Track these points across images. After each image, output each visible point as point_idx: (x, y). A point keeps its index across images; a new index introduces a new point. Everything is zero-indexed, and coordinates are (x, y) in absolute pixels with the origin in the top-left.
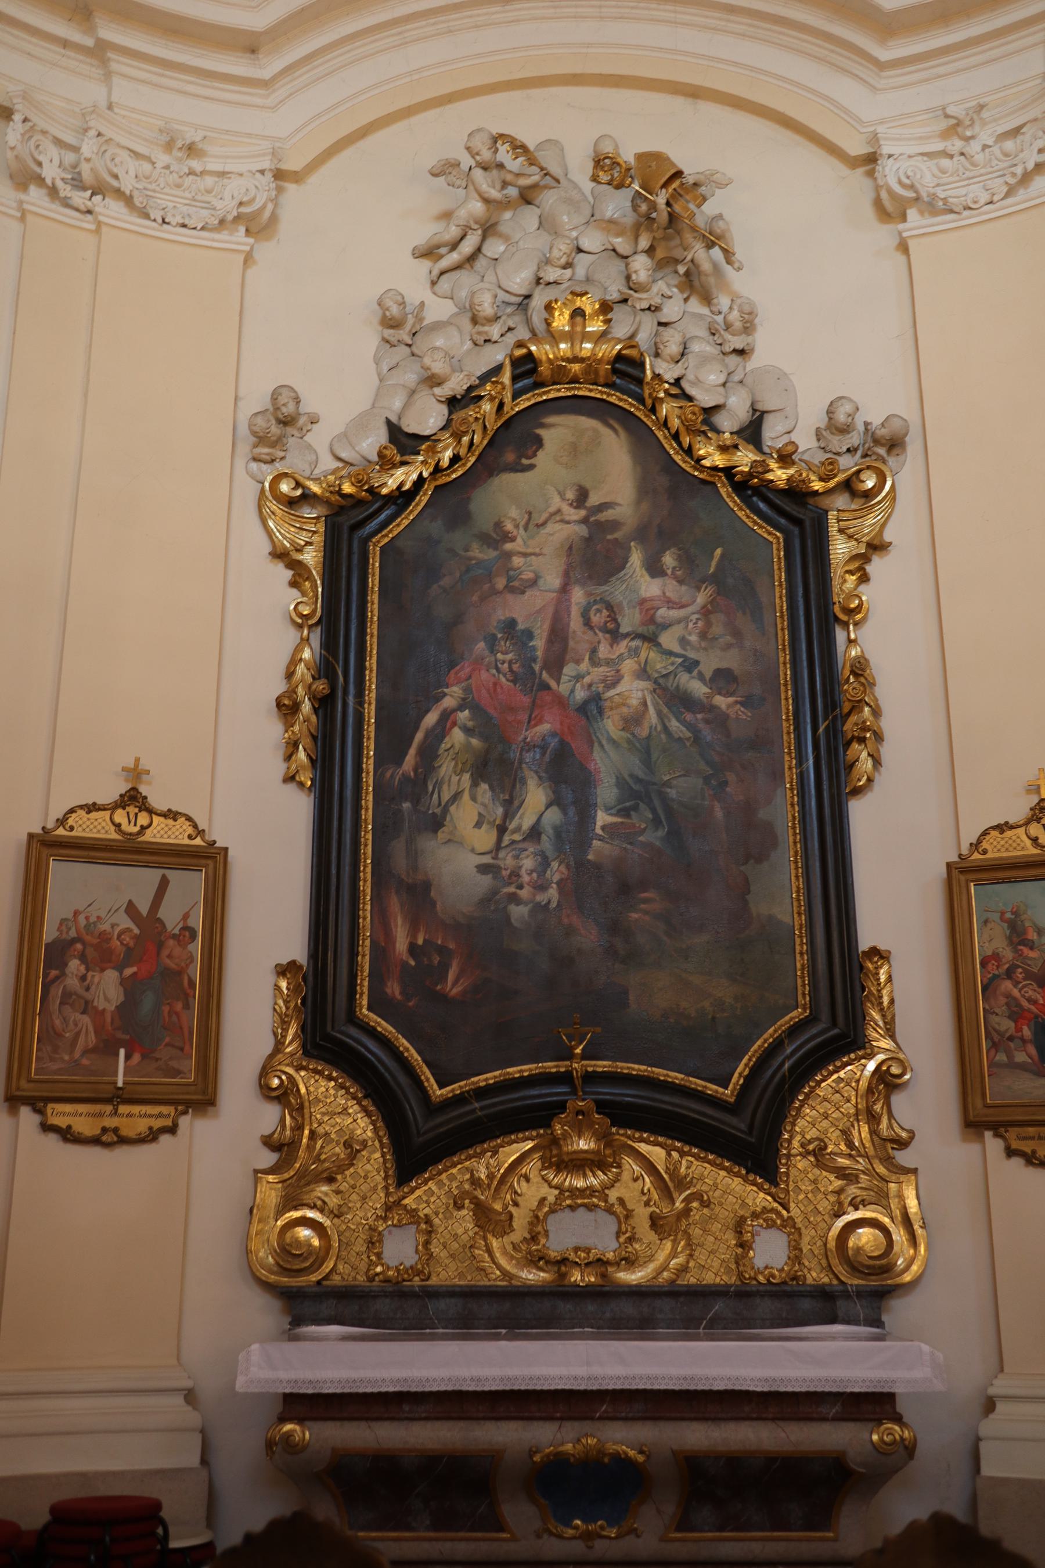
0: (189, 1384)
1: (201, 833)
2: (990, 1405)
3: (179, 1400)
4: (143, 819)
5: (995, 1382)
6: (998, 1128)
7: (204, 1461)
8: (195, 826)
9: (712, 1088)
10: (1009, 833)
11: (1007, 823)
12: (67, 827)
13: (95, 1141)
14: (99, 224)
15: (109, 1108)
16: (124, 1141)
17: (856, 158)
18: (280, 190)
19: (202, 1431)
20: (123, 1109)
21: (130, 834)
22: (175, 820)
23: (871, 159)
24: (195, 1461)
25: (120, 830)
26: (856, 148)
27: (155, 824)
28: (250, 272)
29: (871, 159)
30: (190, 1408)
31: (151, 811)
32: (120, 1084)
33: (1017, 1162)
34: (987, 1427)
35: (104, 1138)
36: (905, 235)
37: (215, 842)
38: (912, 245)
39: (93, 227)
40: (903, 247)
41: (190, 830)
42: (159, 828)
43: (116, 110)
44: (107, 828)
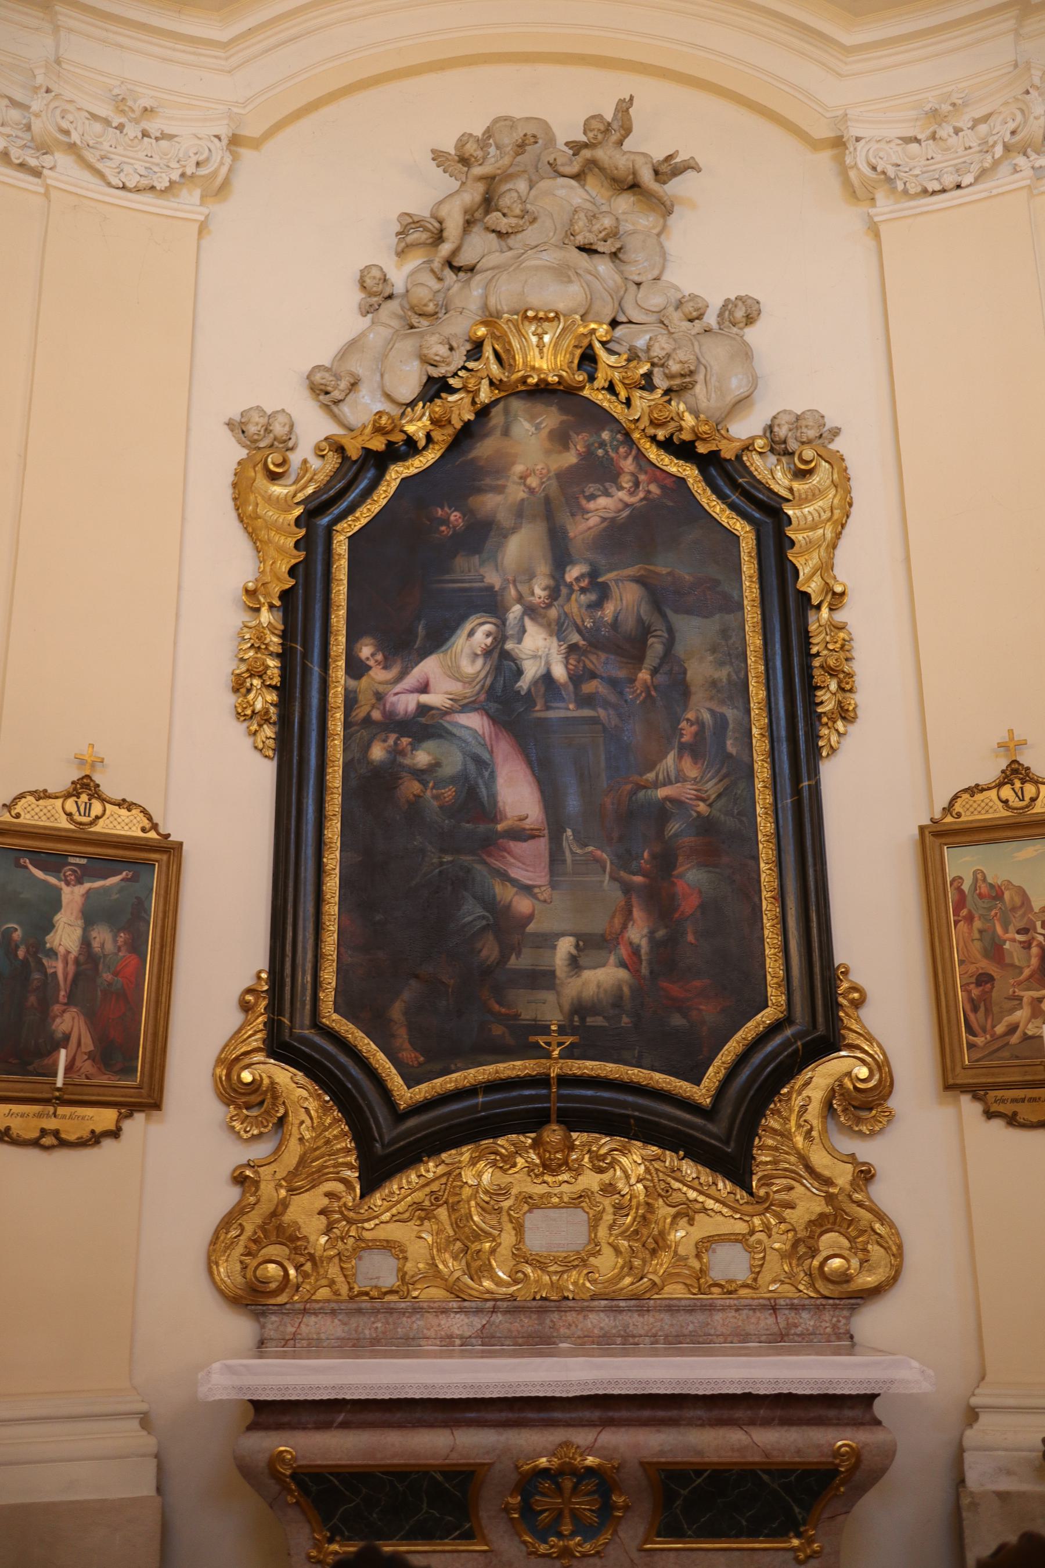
0: (144, 1407)
1: (155, 827)
2: (972, 1415)
3: (135, 1424)
4: (97, 808)
5: (977, 1391)
6: (976, 1092)
7: (159, 1490)
8: (150, 819)
9: (682, 1087)
10: (979, 797)
11: (977, 785)
12: (13, 813)
13: (35, 1143)
14: (47, 187)
15: (51, 1109)
16: (64, 1144)
17: (822, 141)
18: (235, 157)
19: (157, 1456)
20: (62, 1110)
21: (81, 824)
22: (129, 810)
23: (839, 143)
24: (148, 1489)
25: (72, 820)
26: (822, 131)
27: (108, 812)
28: (204, 243)
29: (839, 143)
30: (144, 1433)
31: (103, 800)
32: (59, 1083)
33: (998, 1124)
34: (971, 1436)
35: (44, 1141)
36: (876, 219)
37: (169, 835)
38: (883, 228)
39: (42, 190)
40: (874, 230)
41: (146, 824)
42: (111, 819)
43: (64, 66)
44: (57, 816)
